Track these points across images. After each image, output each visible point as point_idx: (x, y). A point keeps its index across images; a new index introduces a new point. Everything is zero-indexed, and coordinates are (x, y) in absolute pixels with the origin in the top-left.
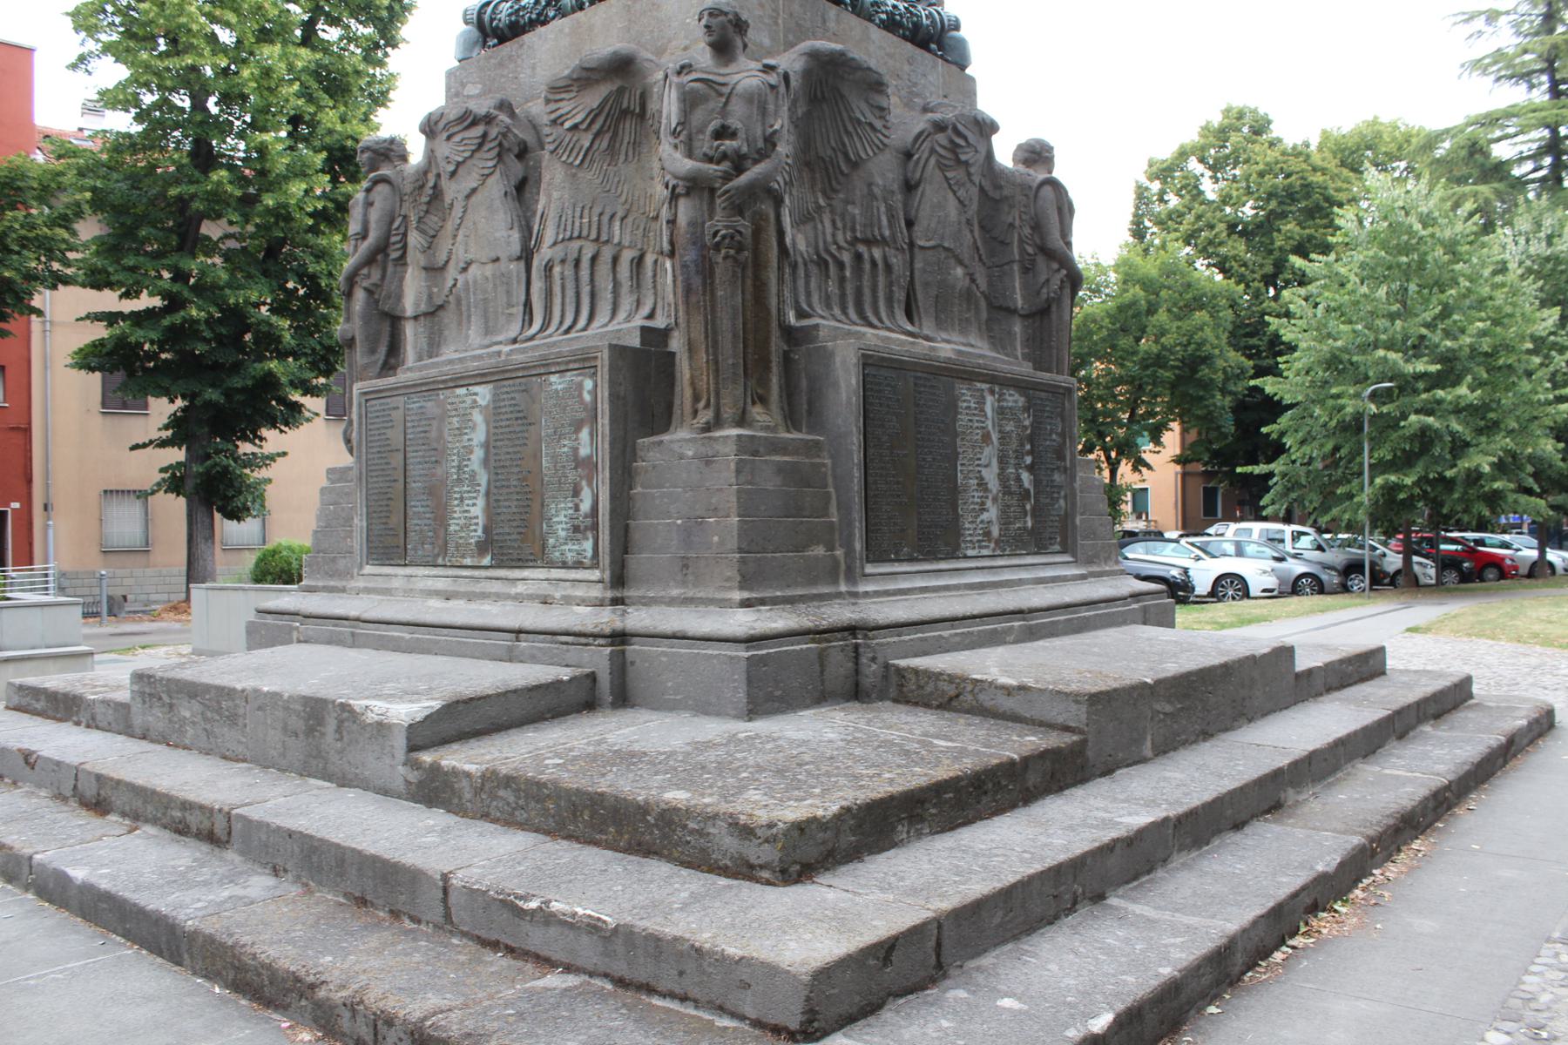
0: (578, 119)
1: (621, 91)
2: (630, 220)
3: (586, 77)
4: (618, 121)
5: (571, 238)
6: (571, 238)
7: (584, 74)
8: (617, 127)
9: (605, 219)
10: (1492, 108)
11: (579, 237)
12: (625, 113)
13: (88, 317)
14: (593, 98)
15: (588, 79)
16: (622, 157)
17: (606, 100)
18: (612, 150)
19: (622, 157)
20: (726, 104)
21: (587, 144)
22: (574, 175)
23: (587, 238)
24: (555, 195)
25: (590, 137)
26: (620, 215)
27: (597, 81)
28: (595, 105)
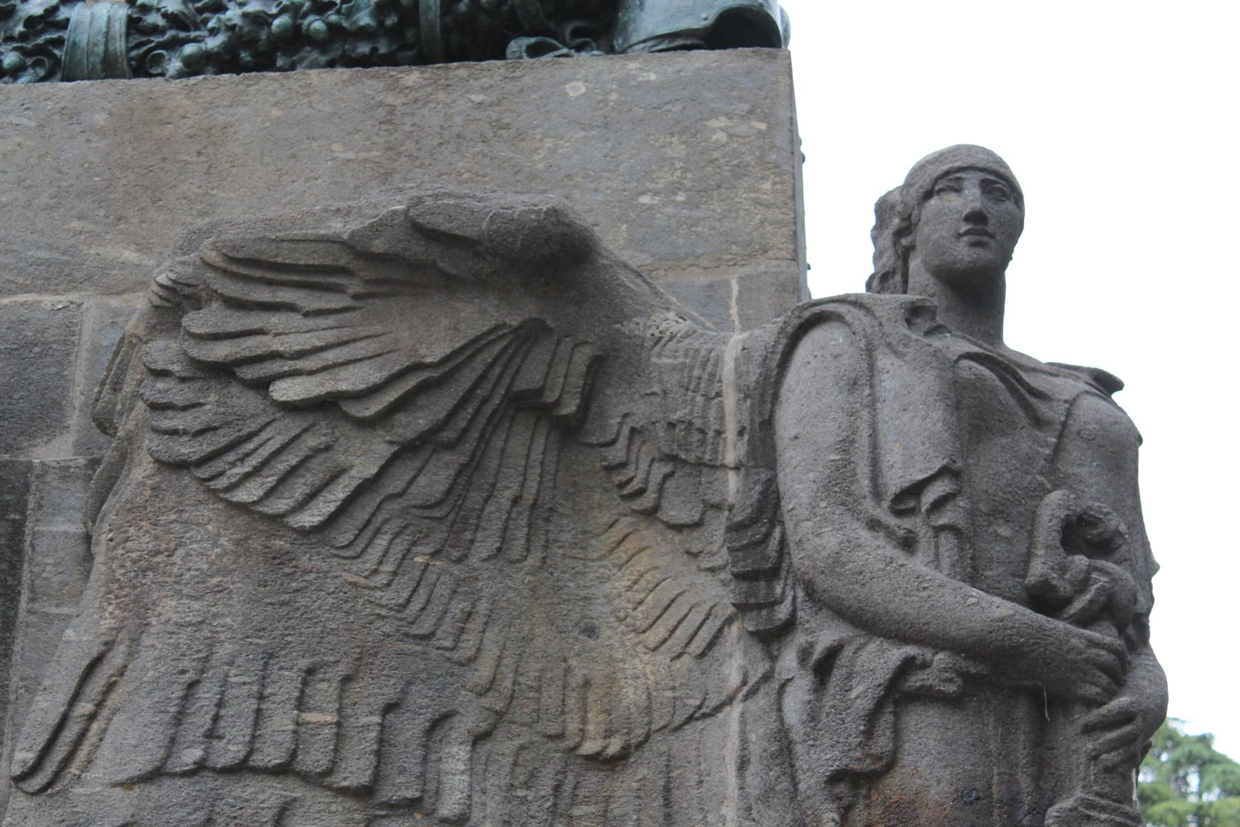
0: (349, 380)
1: (529, 335)
2: (503, 747)
3: (419, 259)
4: (494, 422)
5: (241, 769)
6: (241, 769)
7: (419, 249)
8: (484, 440)
9: (410, 728)
10: (930, 152)
11: (282, 771)
12: (528, 405)
13: (426, 746)
14: (434, 332)
15: (415, 266)
16: (487, 543)
17: (475, 346)
18: (453, 517)
19: (487, 543)
20: (1058, 449)
21: (366, 468)
22: (278, 560)
23: (318, 780)
24: (169, 608)
25: (385, 451)
26: (468, 721)
27: (451, 284)
28: (434, 353)
